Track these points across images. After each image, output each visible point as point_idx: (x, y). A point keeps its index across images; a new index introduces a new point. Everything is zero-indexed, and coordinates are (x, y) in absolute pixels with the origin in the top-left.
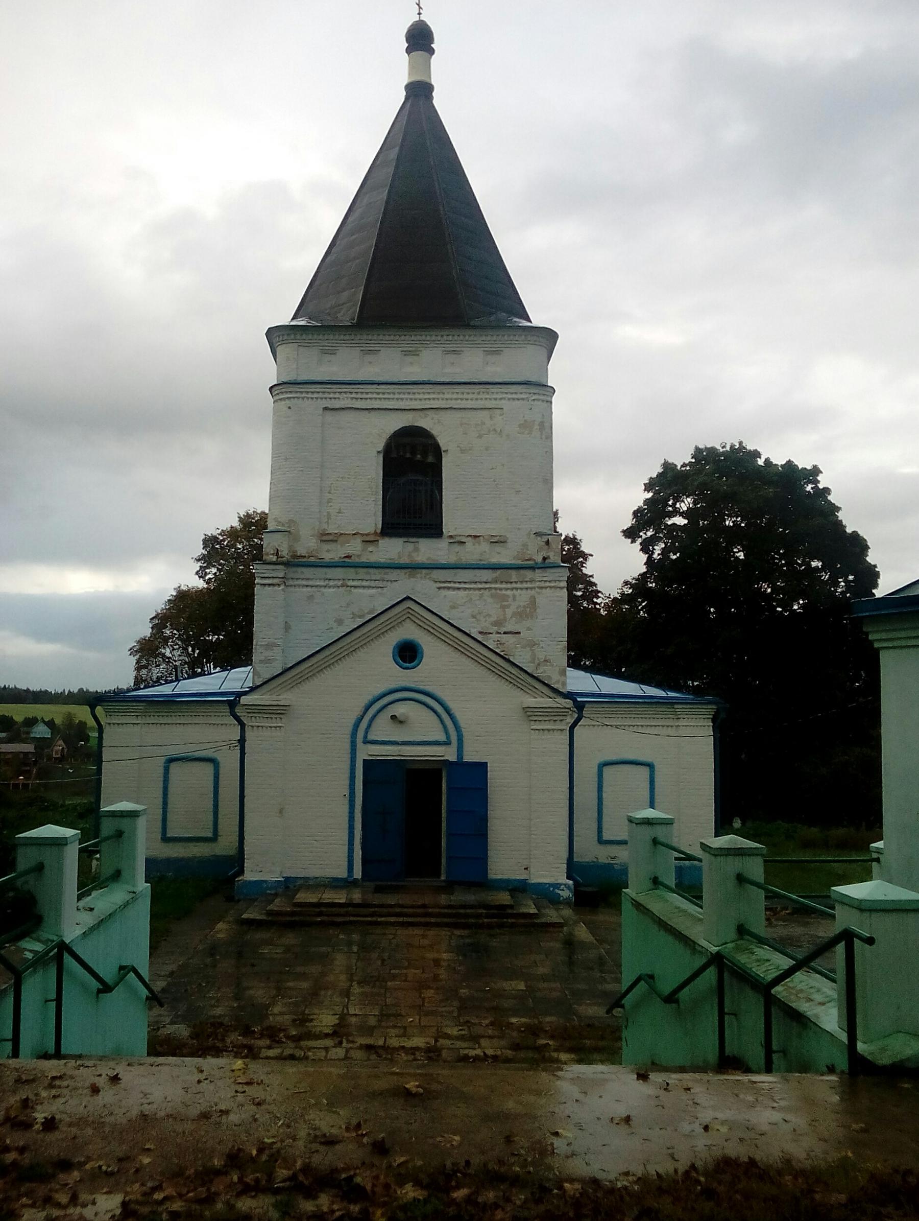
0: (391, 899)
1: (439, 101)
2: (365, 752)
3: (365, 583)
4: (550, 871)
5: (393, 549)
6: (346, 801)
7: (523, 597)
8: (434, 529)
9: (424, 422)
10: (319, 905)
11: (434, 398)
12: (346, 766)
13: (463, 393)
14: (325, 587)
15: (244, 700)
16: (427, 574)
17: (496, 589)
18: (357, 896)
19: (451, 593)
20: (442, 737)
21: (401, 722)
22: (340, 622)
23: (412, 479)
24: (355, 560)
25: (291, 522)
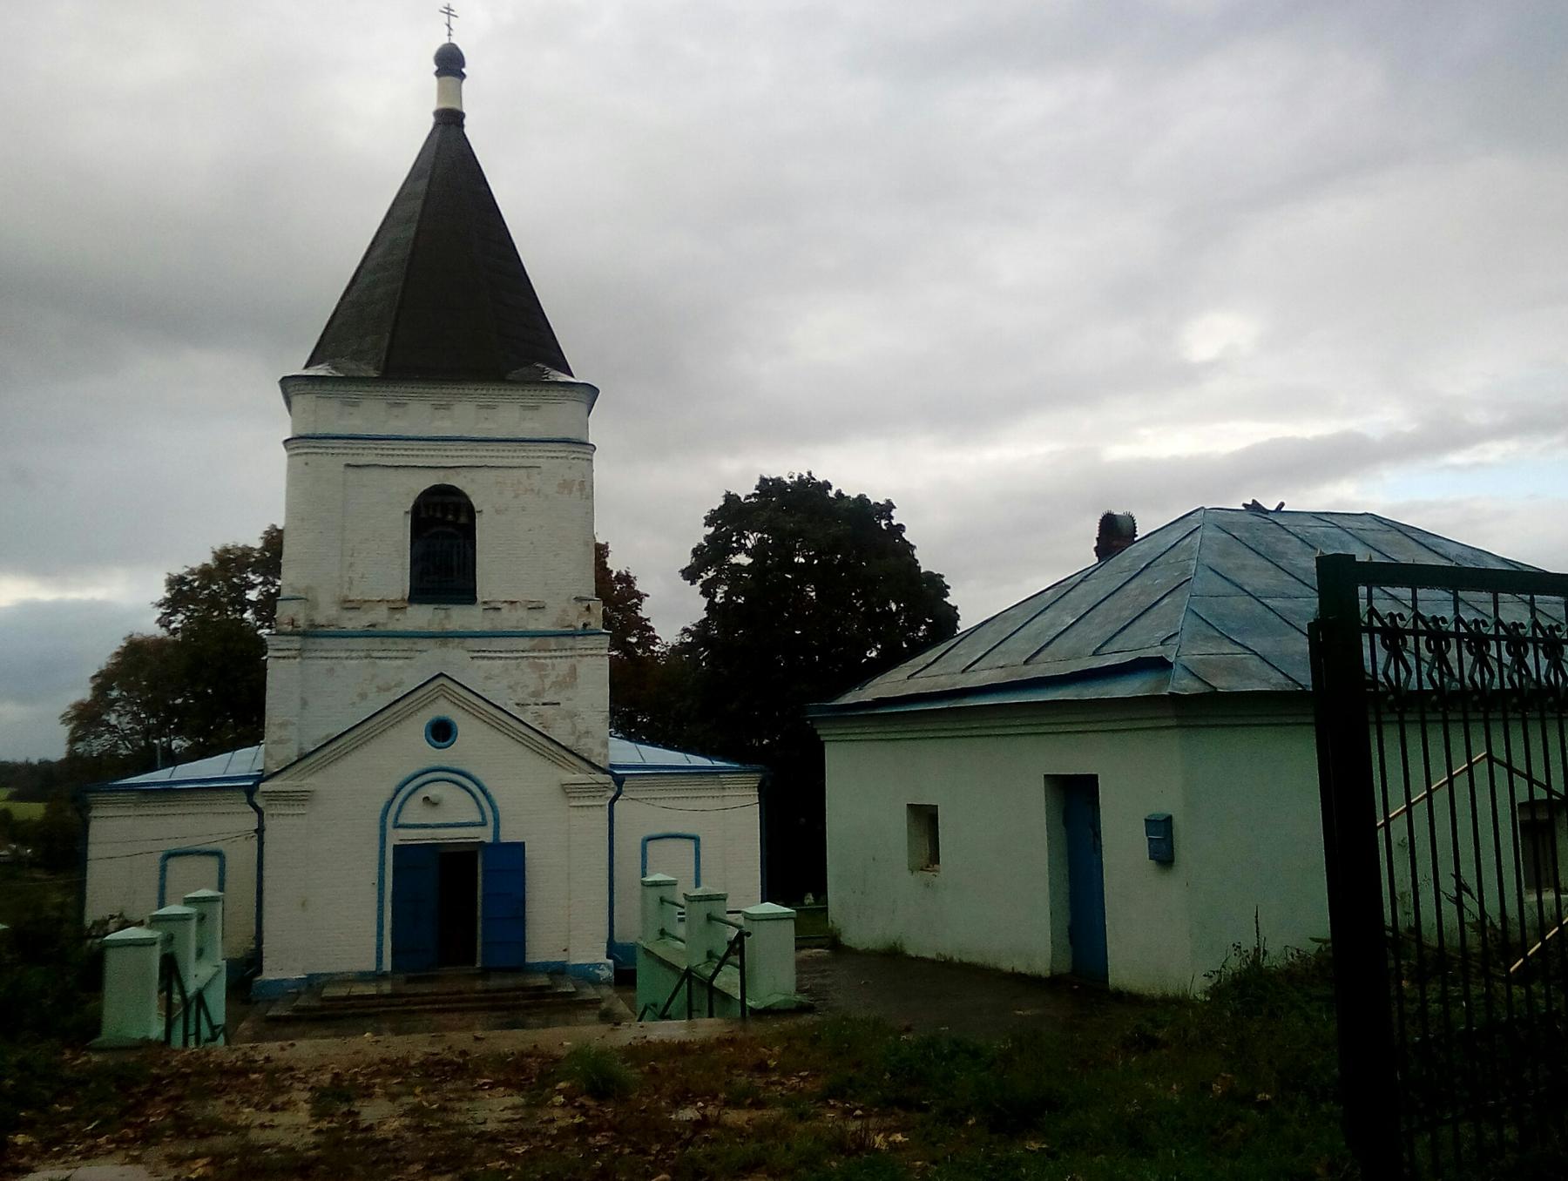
0: (424, 988)
1: (470, 130)
2: (395, 837)
4: (590, 952)
5: (422, 616)
6: (375, 890)
7: (563, 666)
8: (466, 595)
10: (348, 998)
11: (466, 455)
12: (376, 854)
15: (264, 786)
18: (387, 988)
20: (477, 818)
21: (435, 804)
22: (363, 696)
23: (443, 543)
24: (380, 628)
25: (309, 589)
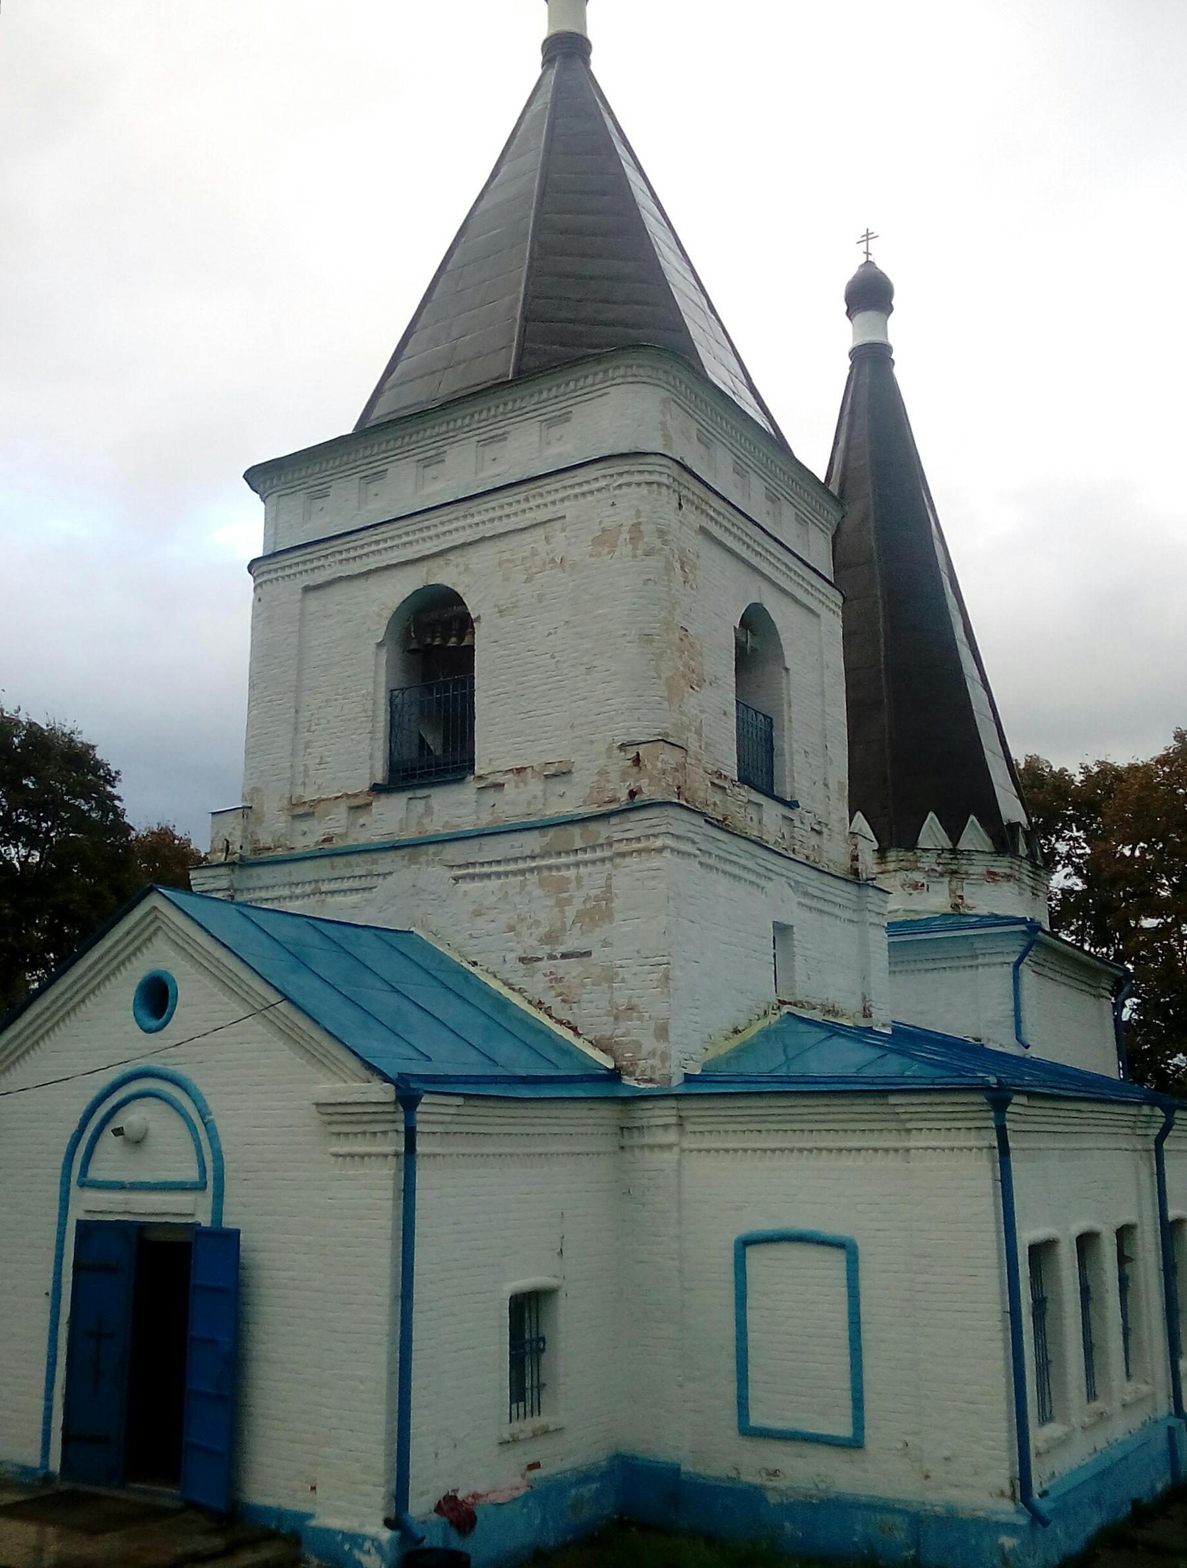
2: (89, 1204)
3: (346, 885)
5: (393, 816)
9: (446, 575)
13: (502, 507)
14: (291, 897)
16: (435, 854)
17: (549, 868)
19: (478, 884)
24: (338, 844)
